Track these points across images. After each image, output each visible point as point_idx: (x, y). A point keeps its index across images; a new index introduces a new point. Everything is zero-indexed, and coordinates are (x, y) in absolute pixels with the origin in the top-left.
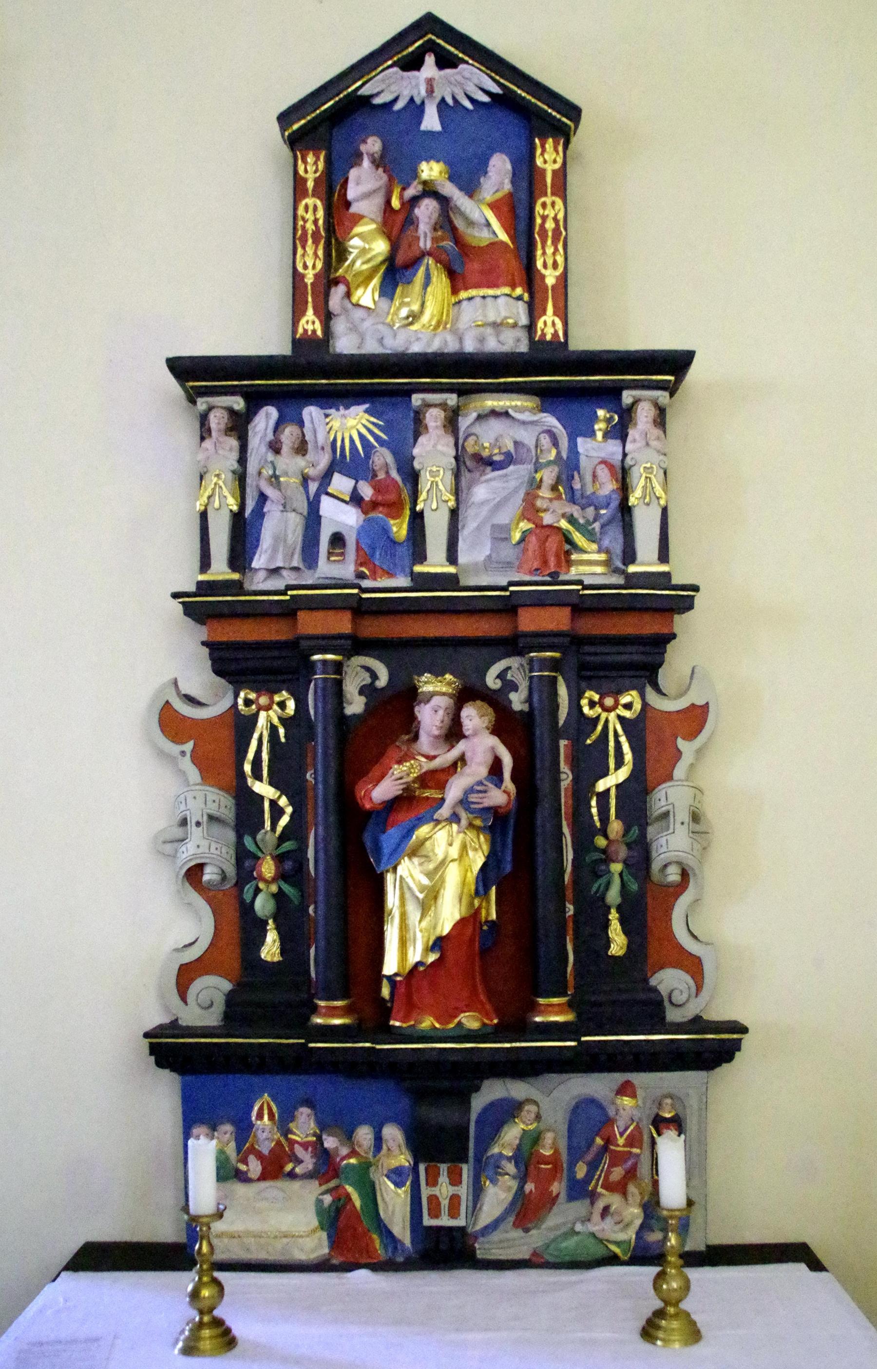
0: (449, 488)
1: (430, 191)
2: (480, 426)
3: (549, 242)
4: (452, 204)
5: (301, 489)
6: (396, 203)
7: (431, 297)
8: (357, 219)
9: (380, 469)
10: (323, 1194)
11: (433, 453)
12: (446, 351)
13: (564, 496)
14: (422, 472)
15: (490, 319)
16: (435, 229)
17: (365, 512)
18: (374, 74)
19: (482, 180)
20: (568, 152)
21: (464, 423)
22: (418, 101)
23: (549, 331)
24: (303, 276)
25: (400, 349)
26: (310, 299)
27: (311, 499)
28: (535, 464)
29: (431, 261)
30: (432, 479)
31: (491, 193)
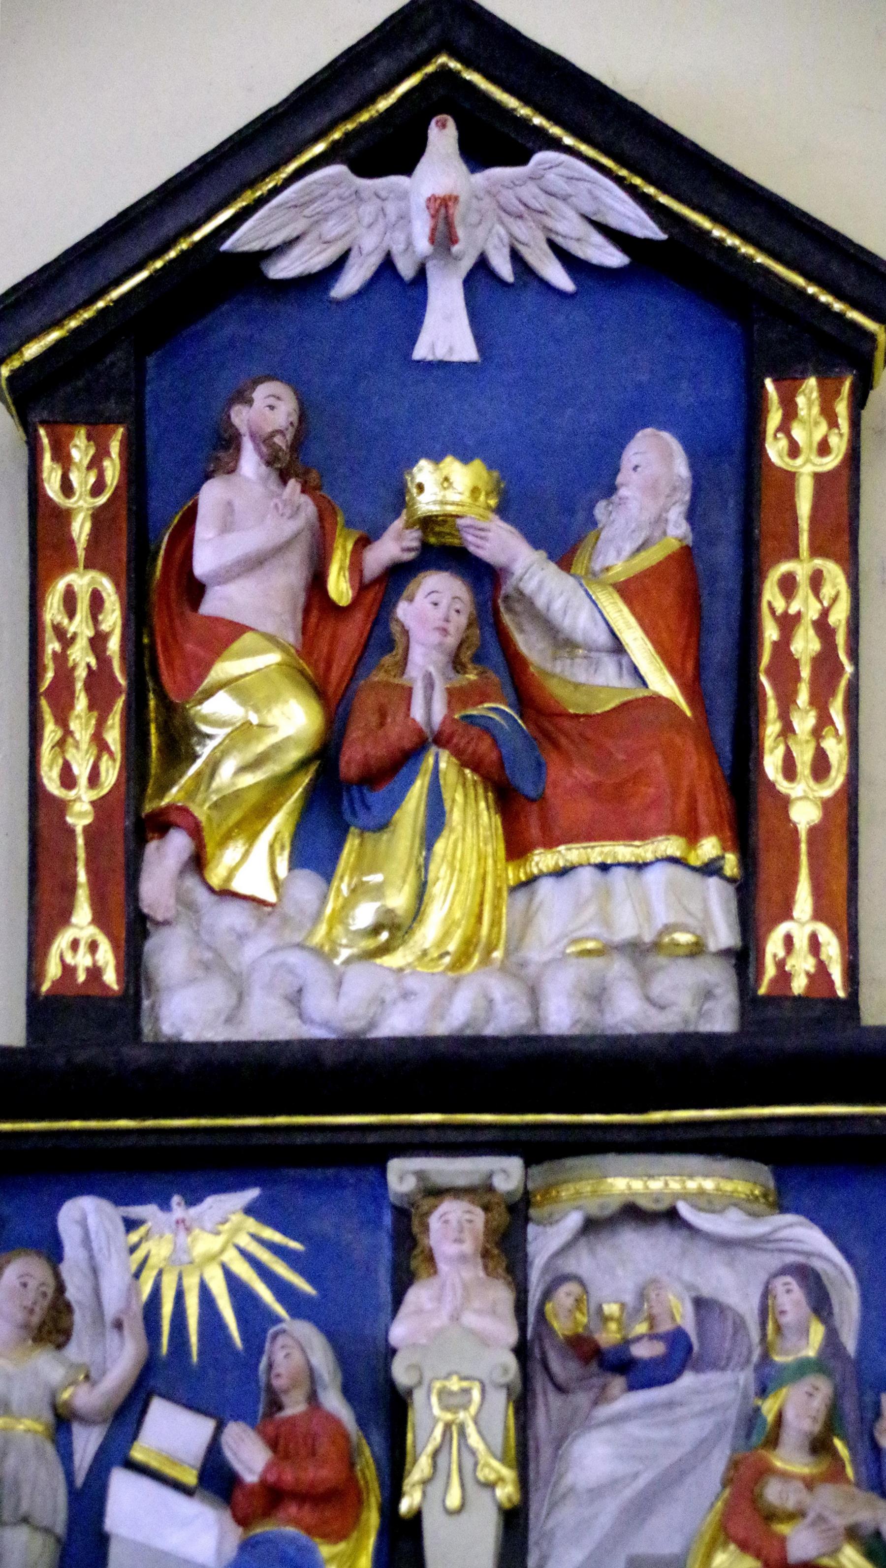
0: (498, 1441)
1: (442, 549)
2: (592, 1252)
3: (803, 696)
4: (507, 588)
5: (50, 1450)
6: (339, 587)
7: (444, 871)
8: (226, 634)
9: (295, 1384)
11: (451, 1336)
12: (489, 1031)
13: (850, 1471)
14: (418, 1397)
15: (617, 933)
16: (457, 664)
17: (243, 1521)
18: (270, 184)
19: (600, 510)
20: (866, 414)
21: (544, 1242)
22: (406, 269)
23: (801, 966)
24: (61, 807)
25: (355, 1026)
26: (82, 876)
27: (80, 1480)
28: (758, 1368)
29: (446, 761)
30: (449, 1416)
31: (628, 548)
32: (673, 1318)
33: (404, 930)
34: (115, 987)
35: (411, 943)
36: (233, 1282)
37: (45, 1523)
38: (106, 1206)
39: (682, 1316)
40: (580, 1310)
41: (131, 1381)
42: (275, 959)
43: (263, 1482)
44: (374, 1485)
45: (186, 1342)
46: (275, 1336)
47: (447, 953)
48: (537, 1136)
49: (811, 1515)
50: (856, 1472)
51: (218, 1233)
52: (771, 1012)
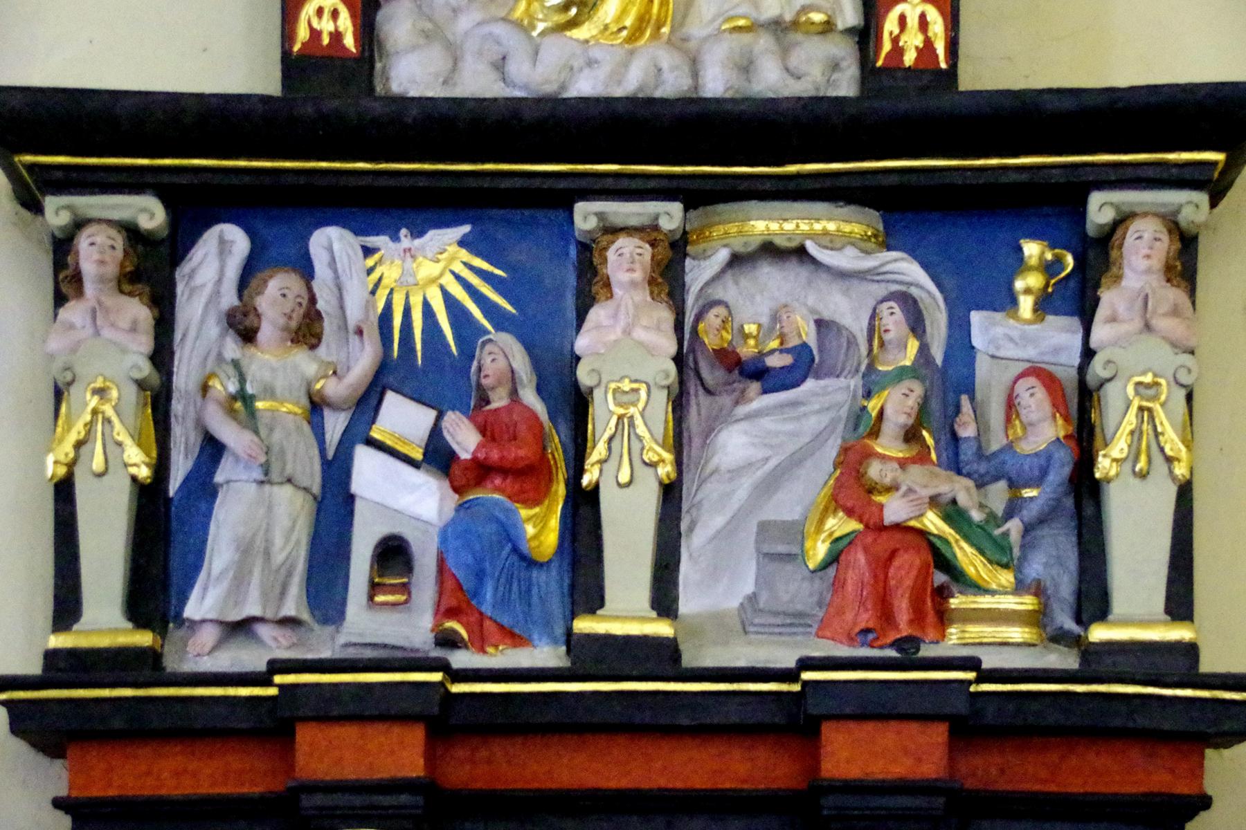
0: (659, 431)
5: (306, 428)
11: (624, 347)
12: (658, 94)
13: (934, 456)
14: (598, 394)
17: (456, 490)
23: (912, 41)
25: (549, 89)
30: (621, 411)
32: (800, 336)
33: (590, 6)
34: (354, 50)
35: (595, 19)
36: (451, 302)
37: (305, 485)
38: (348, 235)
39: (807, 334)
40: (724, 328)
41: (369, 379)
42: (486, 29)
43: (475, 459)
44: (562, 464)
45: (413, 350)
46: (484, 343)
47: (624, 28)
48: (696, 185)
49: (904, 488)
50: (938, 457)
51: (438, 261)
52: (887, 81)
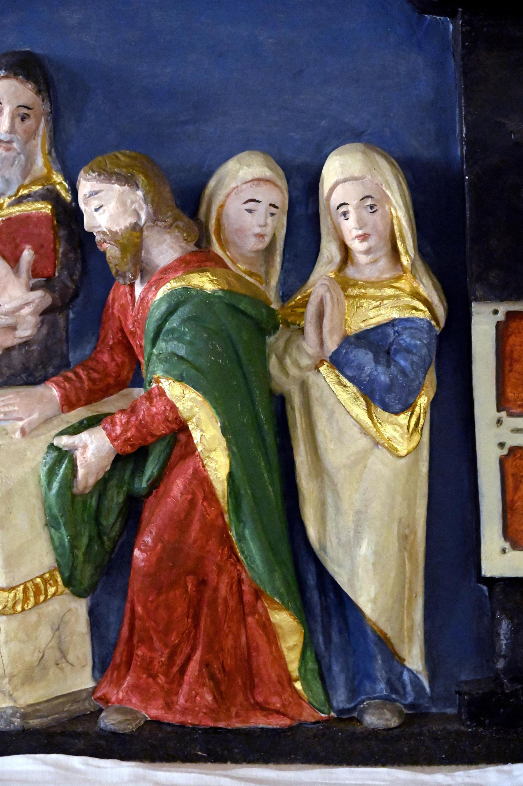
10: (75, 430)
